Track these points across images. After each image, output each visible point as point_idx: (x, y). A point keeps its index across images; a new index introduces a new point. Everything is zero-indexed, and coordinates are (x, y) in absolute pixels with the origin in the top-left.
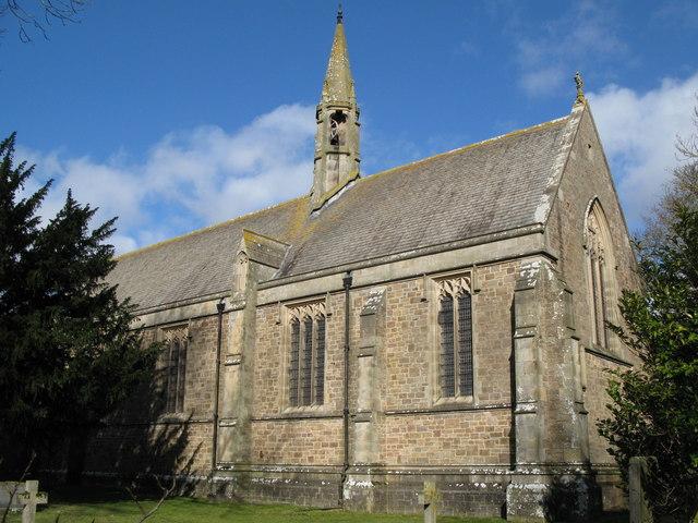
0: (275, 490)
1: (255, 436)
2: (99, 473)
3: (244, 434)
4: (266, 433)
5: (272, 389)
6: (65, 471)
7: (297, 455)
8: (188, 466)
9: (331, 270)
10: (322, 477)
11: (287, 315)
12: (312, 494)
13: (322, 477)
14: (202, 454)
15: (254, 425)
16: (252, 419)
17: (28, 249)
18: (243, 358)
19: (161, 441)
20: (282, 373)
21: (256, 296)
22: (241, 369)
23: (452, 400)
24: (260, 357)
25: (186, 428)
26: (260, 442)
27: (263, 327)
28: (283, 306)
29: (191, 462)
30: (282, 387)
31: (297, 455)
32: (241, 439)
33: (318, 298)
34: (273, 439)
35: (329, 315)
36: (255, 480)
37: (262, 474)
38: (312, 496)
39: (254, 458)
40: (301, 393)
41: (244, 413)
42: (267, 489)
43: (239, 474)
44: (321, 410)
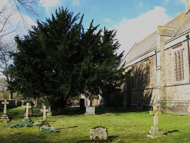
0: (172, 109)
1: (167, 92)
2: (134, 104)
3: (163, 91)
4: (170, 90)
5: (170, 76)
6: (126, 104)
7: (178, 97)
8: (153, 102)
9: (183, 34)
10: (185, 104)
11: (172, 51)
12: (182, 110)
13: (185, 104)
14: (156, 97)
15: (167, 88)
16: (166, 86)
17: (53, 71)
18: (161, 67)
19: (146, 95)
20: (173, 71)
21: (164, 47)
22: (161, 71)
23: (178, 82)
24: (167, 66)
25: (152, 90)
26: (169, 93)
27: (167, 56)
28: (171, 48)
29: (153, 101)
30: (173, 75)
31: (178, 97)
32: (162, 93)
33: (180, 44)
34: (172, 92)
35: (184, 49)
36: (167, 106)
37: (169, 104)
38: (182, 111)
39: (167, 99)
40: (179, 77)
41: (163, 84)
42: (170, 109)
43: (162, 104)
44: (183, 82)
